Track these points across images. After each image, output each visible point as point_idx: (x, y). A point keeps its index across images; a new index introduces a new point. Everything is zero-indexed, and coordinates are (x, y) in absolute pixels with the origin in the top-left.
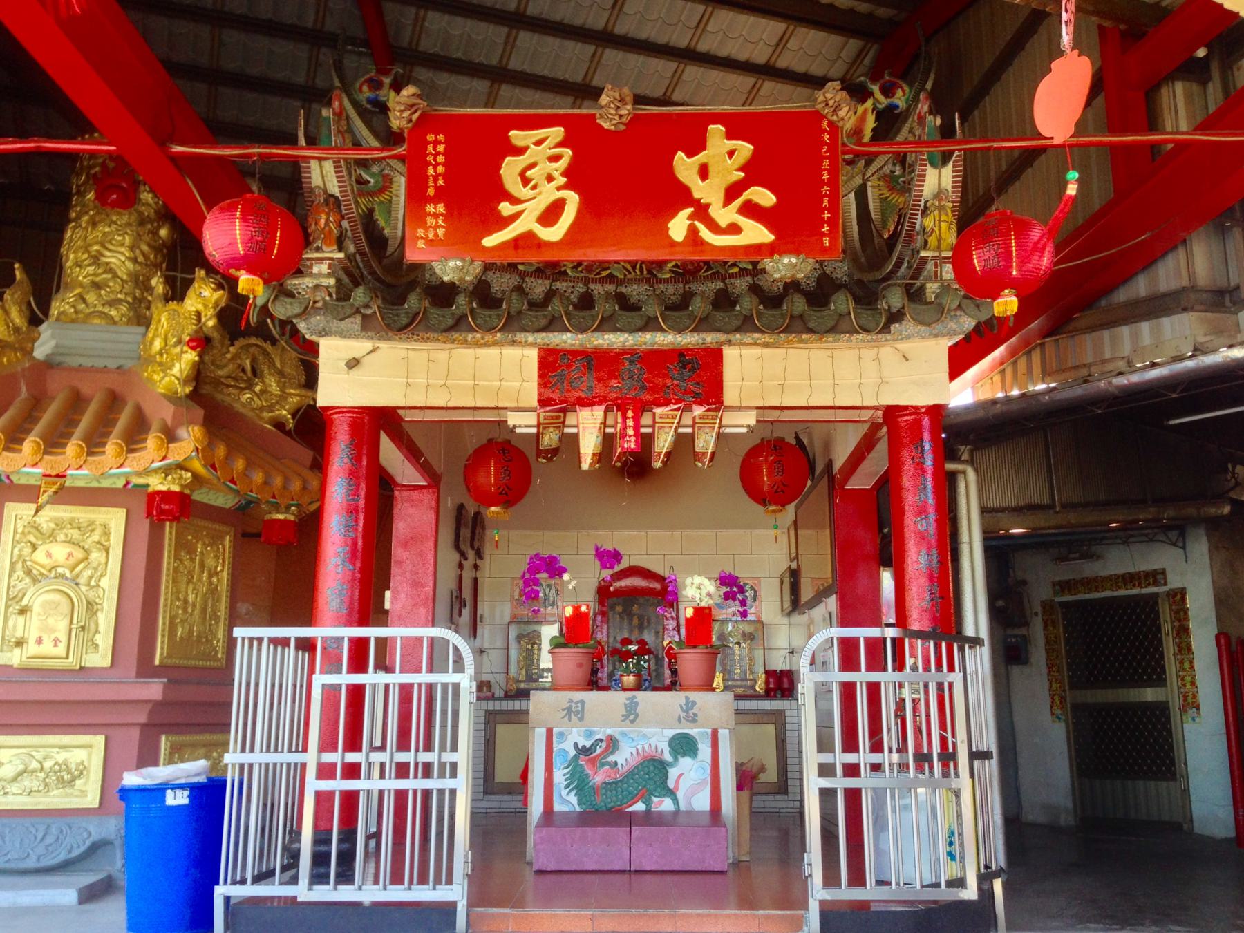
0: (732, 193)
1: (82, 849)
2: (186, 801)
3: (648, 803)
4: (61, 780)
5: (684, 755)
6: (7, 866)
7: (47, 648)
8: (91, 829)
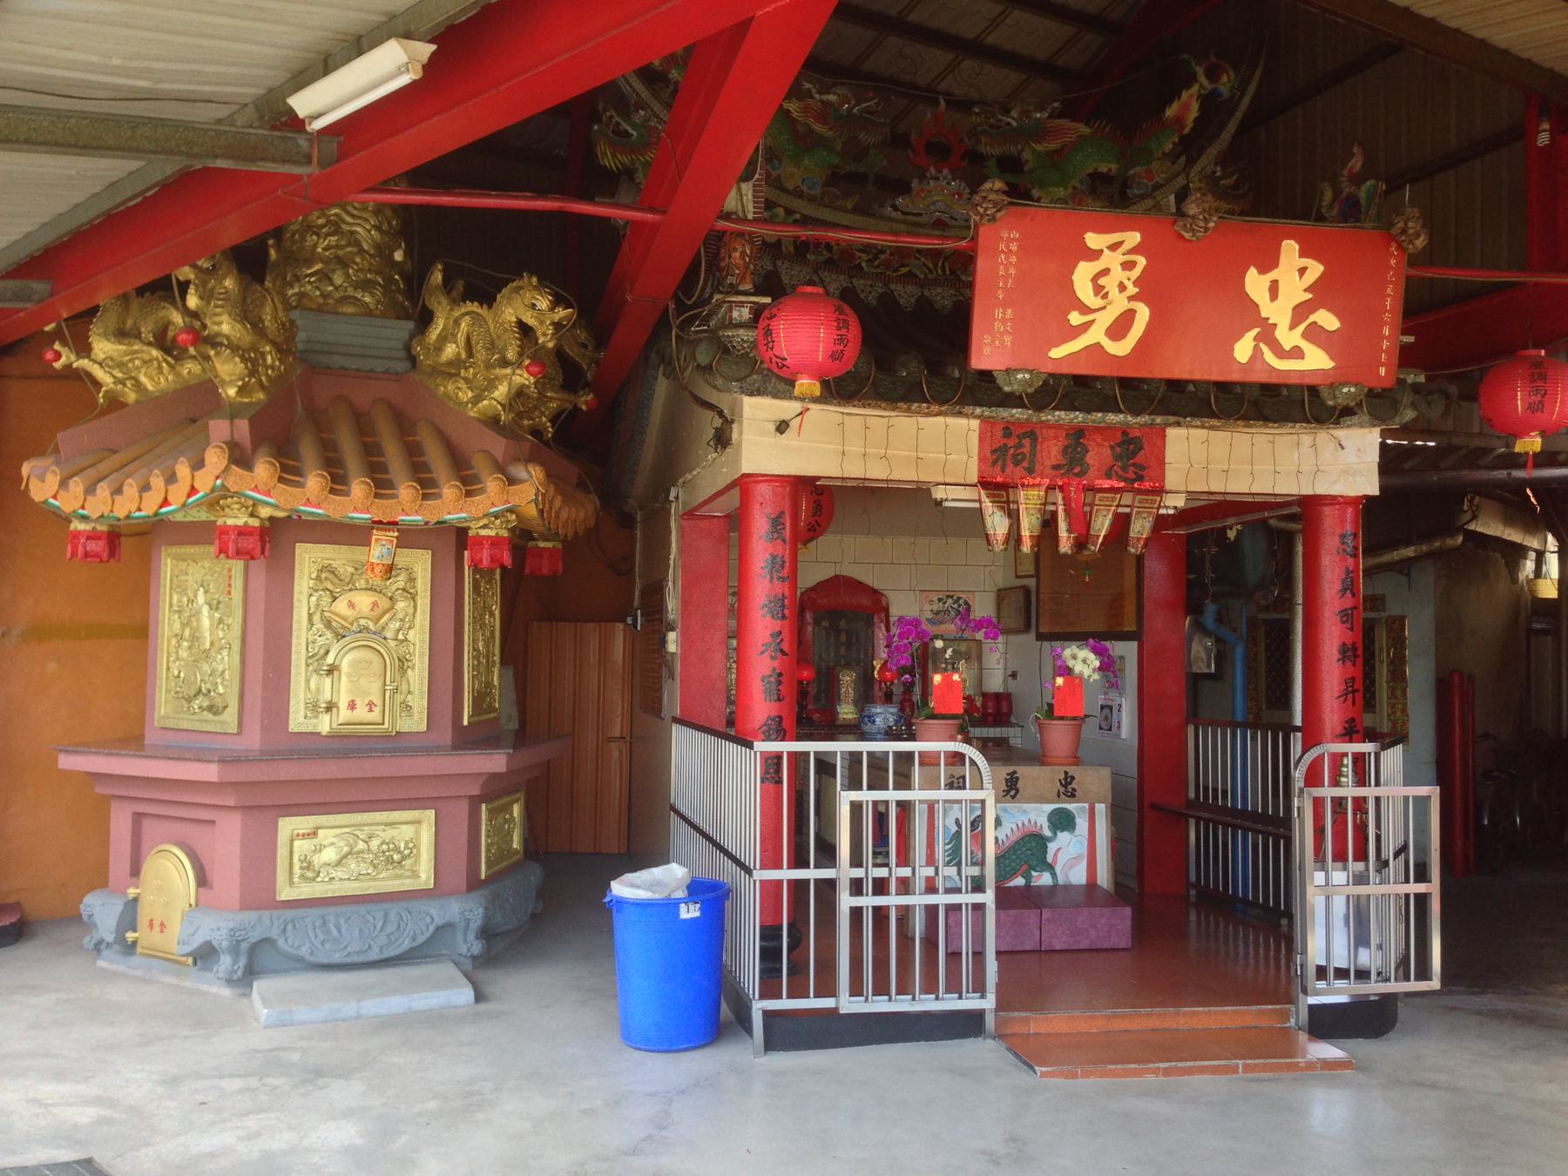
0: (1300, 312)
1: (428, 935)
2: (697, 914)
3: (1028, 877)
4: (390, 861)
5: (1063, 830)
6: (348, 960)
7: (361, 713)
8: (433, 912)
